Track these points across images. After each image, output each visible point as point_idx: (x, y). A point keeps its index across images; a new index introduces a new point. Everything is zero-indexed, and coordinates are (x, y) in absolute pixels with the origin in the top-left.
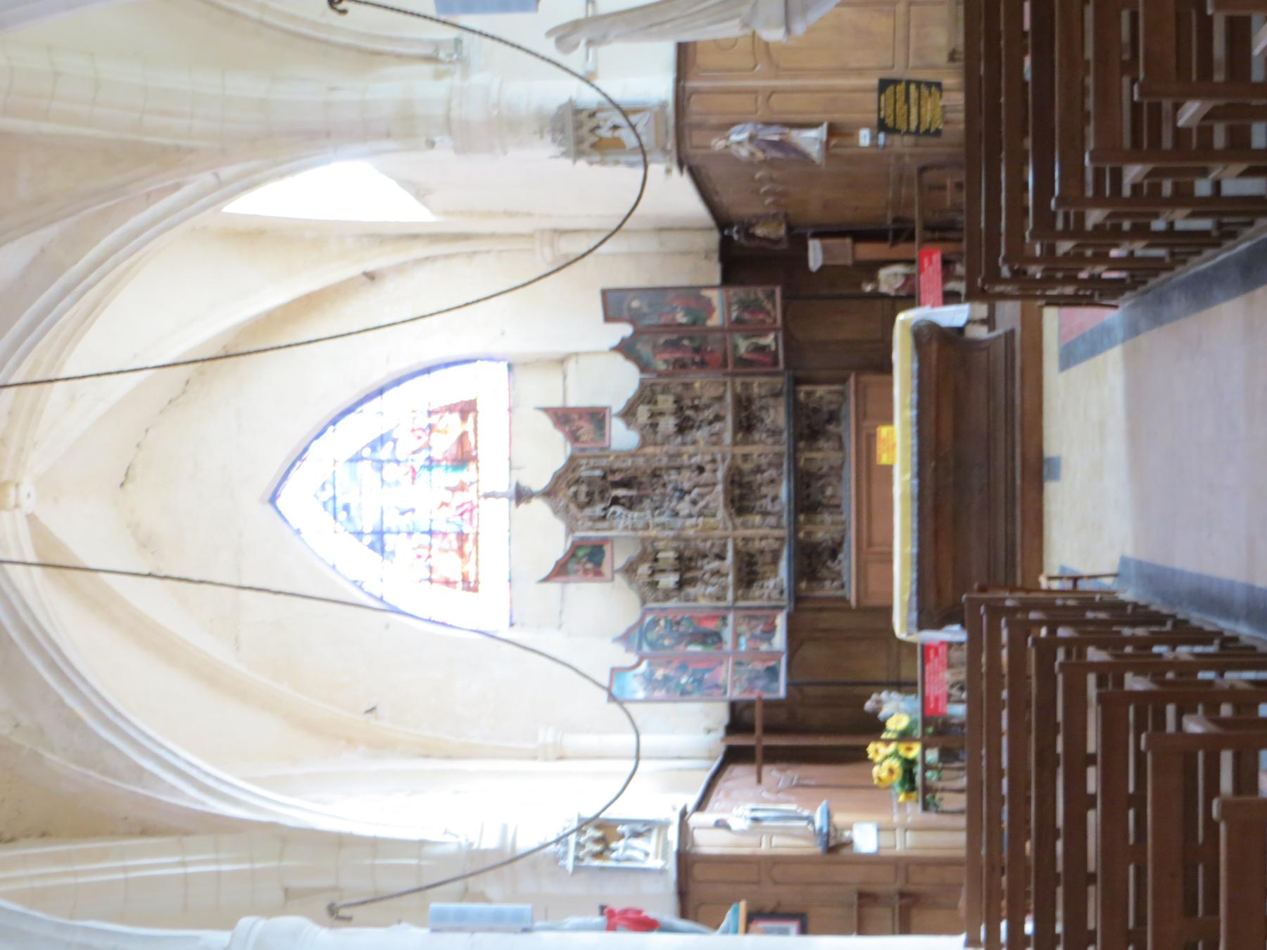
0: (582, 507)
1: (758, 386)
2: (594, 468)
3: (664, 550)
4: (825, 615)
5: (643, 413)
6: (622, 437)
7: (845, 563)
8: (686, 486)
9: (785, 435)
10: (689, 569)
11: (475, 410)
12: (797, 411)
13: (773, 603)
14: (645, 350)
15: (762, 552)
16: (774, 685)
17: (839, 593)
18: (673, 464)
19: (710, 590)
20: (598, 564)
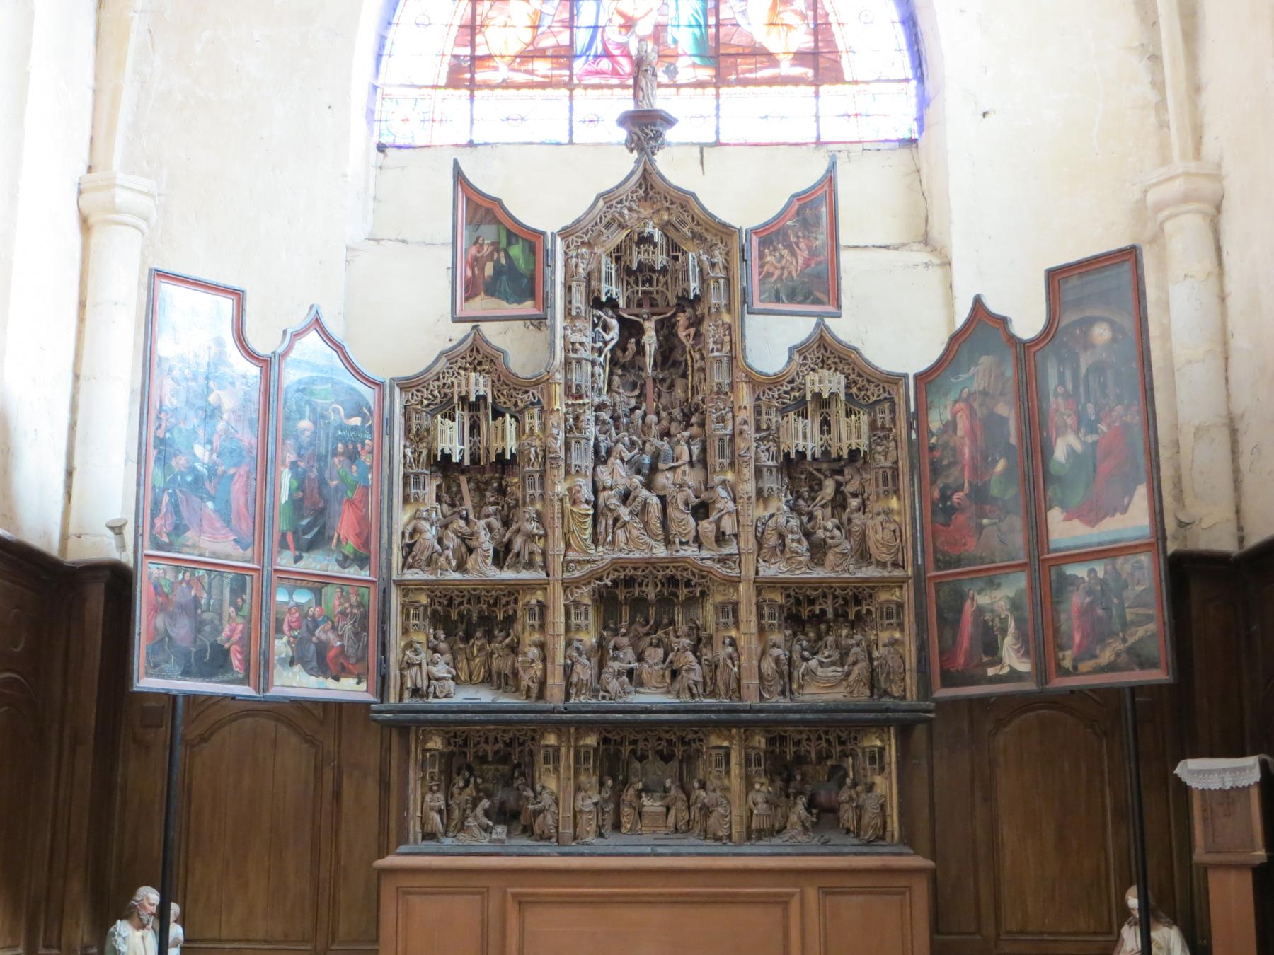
0: (618, 255)
1: (895, 643)
2: (703, 280)
3: (520, 432)
4: (372, 791)
5: (830, 382)
6: (772, 341)
7: (484, 841)
8: (663, 479)
9: (784, 702)
10: (480, 489)
11: (816, 82)
12: (840, 728)
13: (394, 672)
14: (981, 373)
15: (514, 649)
16: (172, 666)
17: (415, 828)
18: (713, 447)
19: (430, 533)
20: (491, 290)
